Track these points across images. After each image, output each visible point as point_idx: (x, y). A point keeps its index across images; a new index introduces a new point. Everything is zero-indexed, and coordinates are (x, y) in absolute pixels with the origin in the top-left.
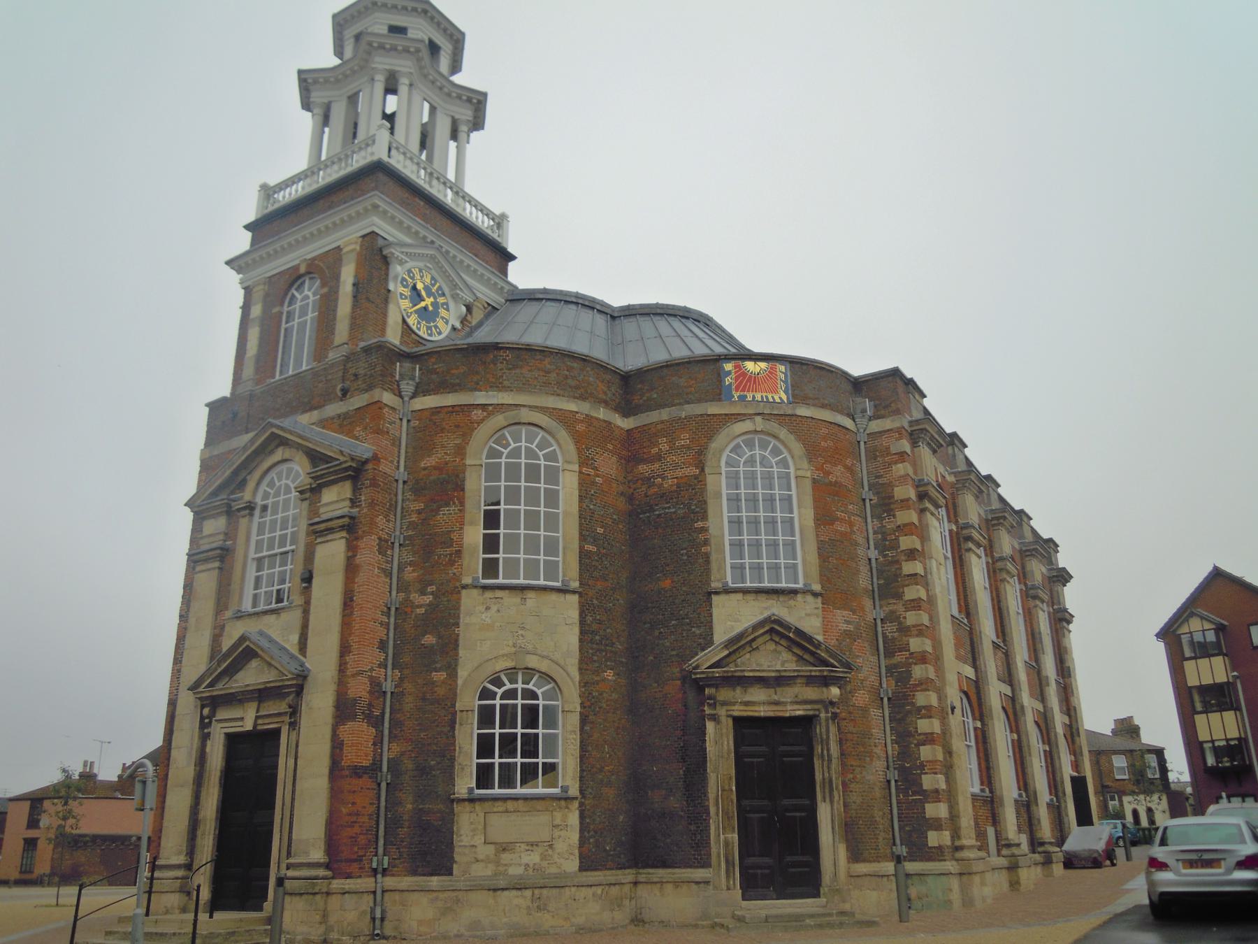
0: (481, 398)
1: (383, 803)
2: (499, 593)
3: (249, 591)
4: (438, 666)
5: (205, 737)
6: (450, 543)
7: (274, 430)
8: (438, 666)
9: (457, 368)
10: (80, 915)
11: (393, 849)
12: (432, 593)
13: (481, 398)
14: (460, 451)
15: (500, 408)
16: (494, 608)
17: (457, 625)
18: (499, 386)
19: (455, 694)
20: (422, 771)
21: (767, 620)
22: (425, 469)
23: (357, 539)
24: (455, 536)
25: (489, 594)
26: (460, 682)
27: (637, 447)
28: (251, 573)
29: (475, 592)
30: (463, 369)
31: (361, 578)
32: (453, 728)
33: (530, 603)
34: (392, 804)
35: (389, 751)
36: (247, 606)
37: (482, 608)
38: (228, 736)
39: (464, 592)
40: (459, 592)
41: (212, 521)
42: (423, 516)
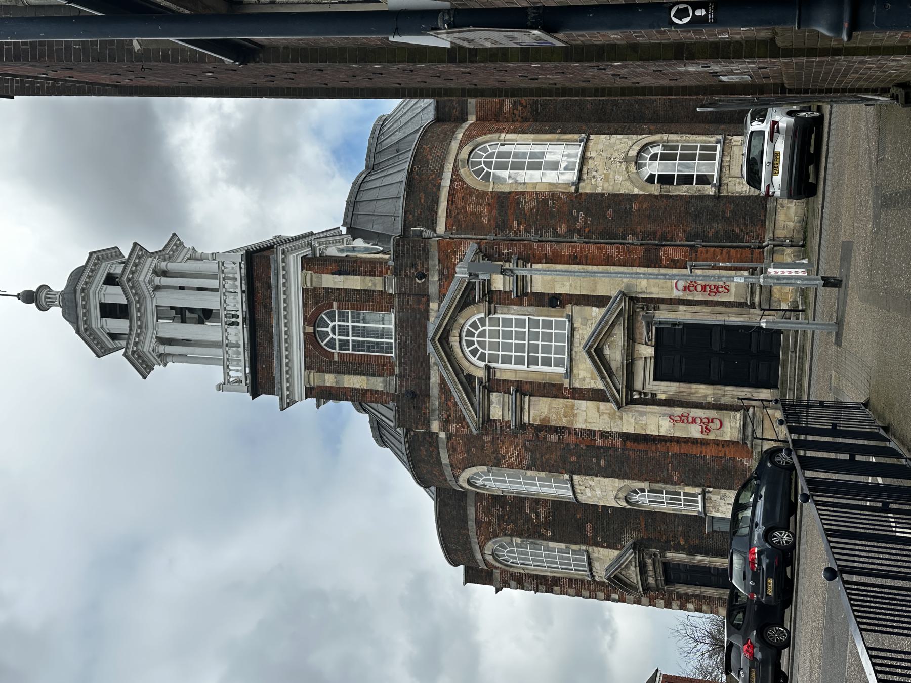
0: (446, 182)
1: (716, 244)
2: (585, 170)
3: (552, 369)
4: (628, 207)
5: (653, 401)
6: (545, 201)
7: (437, 338)
8: (628, 207)
9: (420, 199)
10: (775, 438)
11: (747, 237)
12: (578, 212)
13: (446, 182)
14: (481, 195)
15: (455, 171)
16: (594, 173)
17: (603, 195)
18: (440, 173)
19: (649, 195)
20: (697, 216)
21: (475, 575)
22: (489, 220)
23: (534, 256)
24: (541, 198)
25: (585, 177)
26: (641, 193)
27: (489, 113)
28: (539, 368)
29: (581, 184)
30: (422, 195)
31: (590, 164)
32: (671, 196)
33: (593, 154)
34: (716, 238)
35: (680, 239)
36: (562, 370)
37: (593, 180)
38: (655, 380)
39: (580, 191)
40: (581, 194)
41: (492, 408)
42: (523, 221)
